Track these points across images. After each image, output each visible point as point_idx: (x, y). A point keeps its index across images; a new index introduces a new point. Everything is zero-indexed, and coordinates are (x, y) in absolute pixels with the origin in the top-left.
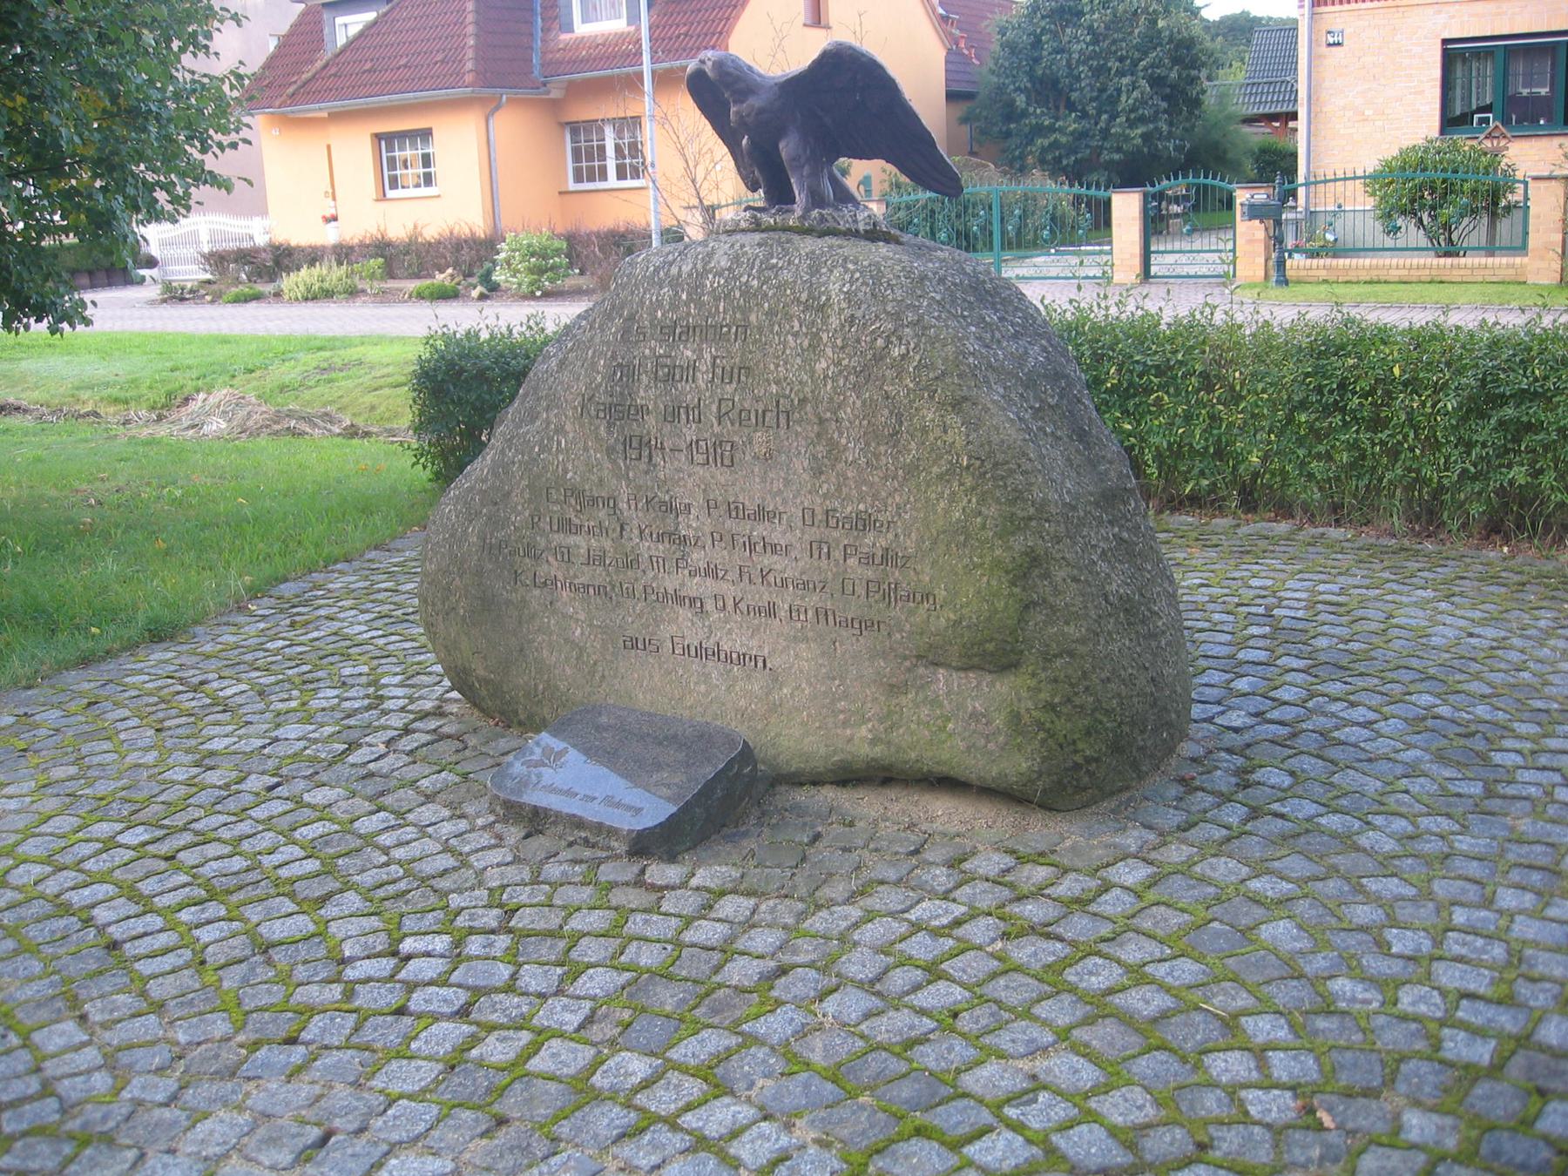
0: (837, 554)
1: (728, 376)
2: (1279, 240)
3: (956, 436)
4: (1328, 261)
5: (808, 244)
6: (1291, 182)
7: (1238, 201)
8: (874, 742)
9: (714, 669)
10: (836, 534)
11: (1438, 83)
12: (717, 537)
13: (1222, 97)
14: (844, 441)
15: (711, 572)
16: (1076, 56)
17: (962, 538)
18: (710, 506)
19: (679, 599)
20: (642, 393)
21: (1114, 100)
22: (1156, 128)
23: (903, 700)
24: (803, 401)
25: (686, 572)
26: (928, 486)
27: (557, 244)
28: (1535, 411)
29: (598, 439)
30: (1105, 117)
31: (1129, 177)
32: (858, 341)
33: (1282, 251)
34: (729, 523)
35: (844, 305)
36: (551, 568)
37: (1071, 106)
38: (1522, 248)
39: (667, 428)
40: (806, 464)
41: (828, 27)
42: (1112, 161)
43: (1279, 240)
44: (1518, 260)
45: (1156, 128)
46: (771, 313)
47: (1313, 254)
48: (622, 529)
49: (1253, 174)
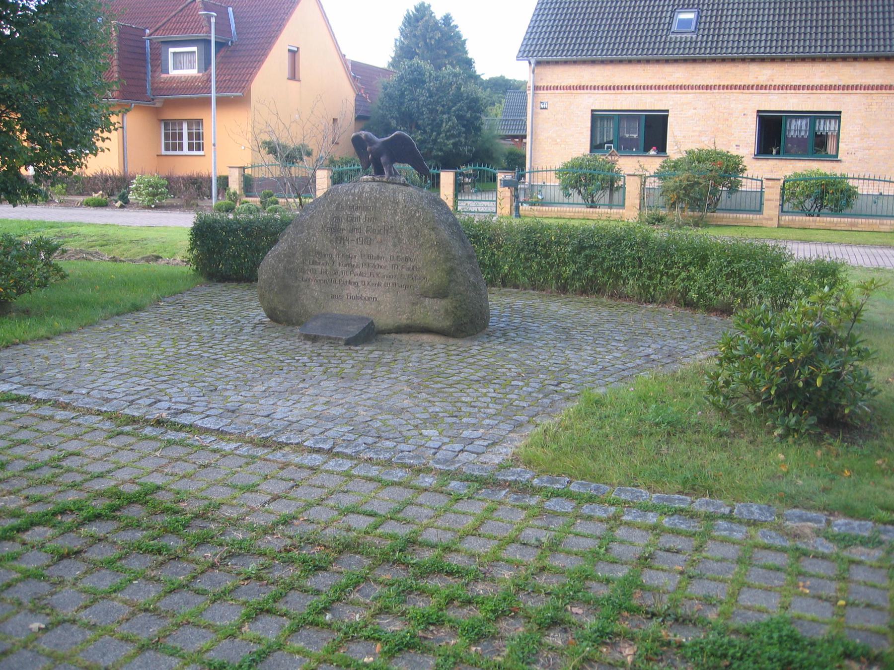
0: (400, 268)
1: (370, 220)
2: (517, 197)
3: (433, 236)
4: (539, 208)
5: (391, 186)
6: (523, 170)
7: (499, 178)
8: (408, 319)
11: (589, 129)
12: (364, 264)
13: (491, 128)
15: (361, 274)
16: (421, 103)
19: (350, 283)
21: (439, 126)
27: (163, 182)
28: (594, 252)
29: (327, 238)
30: (435, 133)
31: (447, 165)
33: (518, 202)
36: (309, 275)
37: (418, 127)
38: (623, 206)
41: (299, 81)
42: (438, 156)
43: (517, 197)
44: (621, 211)
46: (383, 204)
47: (533, 204)
49: (505, 165)
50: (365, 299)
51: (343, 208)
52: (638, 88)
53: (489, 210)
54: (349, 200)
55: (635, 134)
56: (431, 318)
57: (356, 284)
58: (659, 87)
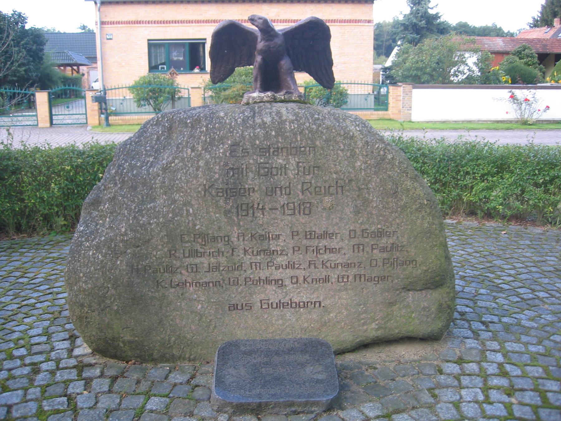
0: (368, 249)
9: (288, 313)
10: (367, 240)
11: (147, 54)
14: (371, 198)
15: (291, 265)
18: (294, 234)
19: (268, 281)
20: (250, 182)
22: (29, 68)
23: (394, 308)
24: (351, 181)
25: (273, 268)
26: (412, 214)
32: (372, 152)
34: (305, 242)
35: (362, 137)
39: (267, 199)
40: (352, 209)
46: (327, 141)
50: (298, 305)
51: (246, 152)
52: (182, 22)
53: (80, 121)
54: (256, 137)
55: (178, 56)
57: (279, 283)
58: (198, 22)
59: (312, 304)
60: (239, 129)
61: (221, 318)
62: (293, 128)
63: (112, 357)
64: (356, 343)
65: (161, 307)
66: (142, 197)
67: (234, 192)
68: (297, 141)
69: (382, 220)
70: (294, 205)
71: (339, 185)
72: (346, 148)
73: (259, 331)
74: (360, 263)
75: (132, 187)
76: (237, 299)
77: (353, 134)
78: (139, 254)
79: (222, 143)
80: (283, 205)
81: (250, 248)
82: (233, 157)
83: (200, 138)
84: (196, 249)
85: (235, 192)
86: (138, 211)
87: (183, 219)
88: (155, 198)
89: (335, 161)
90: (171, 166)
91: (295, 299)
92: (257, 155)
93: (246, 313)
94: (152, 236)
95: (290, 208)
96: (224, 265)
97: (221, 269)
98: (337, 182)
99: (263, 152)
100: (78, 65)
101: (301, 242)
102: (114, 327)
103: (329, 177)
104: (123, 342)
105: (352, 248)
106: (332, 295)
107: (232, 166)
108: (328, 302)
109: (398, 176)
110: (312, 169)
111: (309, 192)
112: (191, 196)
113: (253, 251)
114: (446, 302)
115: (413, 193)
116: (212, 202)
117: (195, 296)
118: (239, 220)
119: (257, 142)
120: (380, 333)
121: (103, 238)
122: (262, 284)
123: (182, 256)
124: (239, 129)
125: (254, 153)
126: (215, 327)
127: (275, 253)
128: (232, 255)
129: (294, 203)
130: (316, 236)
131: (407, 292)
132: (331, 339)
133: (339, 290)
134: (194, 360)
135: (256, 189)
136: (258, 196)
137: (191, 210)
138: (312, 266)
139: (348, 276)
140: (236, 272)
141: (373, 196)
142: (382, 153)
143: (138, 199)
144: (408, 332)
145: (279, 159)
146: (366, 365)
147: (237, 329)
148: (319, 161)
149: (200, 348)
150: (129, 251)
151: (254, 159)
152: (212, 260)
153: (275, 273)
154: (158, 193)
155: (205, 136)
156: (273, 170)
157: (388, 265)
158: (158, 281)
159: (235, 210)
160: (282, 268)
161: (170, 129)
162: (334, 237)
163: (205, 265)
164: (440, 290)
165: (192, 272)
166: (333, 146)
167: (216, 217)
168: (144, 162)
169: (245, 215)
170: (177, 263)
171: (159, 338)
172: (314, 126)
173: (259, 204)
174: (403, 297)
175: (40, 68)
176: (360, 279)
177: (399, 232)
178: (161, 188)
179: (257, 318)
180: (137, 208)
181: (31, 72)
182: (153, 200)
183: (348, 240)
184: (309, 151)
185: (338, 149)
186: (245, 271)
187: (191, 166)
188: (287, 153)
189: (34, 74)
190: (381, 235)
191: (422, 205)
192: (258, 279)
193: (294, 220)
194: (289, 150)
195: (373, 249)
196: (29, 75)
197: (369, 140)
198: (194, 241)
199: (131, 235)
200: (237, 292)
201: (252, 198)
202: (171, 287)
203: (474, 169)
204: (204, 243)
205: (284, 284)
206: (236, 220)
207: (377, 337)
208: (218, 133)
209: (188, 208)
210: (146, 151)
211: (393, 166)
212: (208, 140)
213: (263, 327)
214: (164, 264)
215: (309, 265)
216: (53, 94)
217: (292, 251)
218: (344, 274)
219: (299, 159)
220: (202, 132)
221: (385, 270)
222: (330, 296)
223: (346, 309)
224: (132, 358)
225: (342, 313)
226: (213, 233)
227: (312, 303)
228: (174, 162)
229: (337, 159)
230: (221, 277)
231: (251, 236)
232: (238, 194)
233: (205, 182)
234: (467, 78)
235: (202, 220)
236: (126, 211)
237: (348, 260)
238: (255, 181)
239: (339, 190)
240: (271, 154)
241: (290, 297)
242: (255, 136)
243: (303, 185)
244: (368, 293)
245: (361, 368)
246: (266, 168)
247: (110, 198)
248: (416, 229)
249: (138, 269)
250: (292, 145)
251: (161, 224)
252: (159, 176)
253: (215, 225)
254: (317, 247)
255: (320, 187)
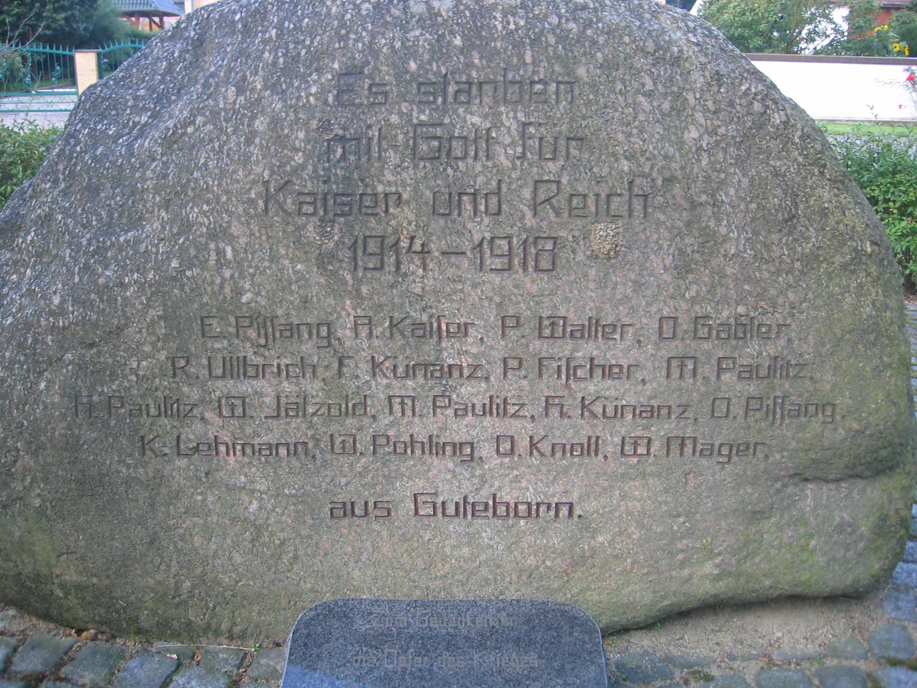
0: (707, 370)
10: (706, 346)
14: (723, 230)
17: (872, 337)
19: (435, 447)
20: (389, 177)
22: (73, 15)
23: (766, 525)
24: (669, 181)
25: (450, 412)
32: (731, 104)
34: (536, 345)
35: (703, 59)
40: (668, 261)
45: (73, 15)
46: (608, 66)
48: (341, 364)
51: (379, 91)
54: (410, 51)
56: (820, 559)
59: (549, 508)
60: (364, 29)
61: (310, 537)
62: (512, 27)
63: (46, 617)
64: (659, 611)
65: (152, 505)
66: (110, 216)
67: (344, 204)
68: (525, 64)
69: (749, 293)
70: (509, 243)
71: (636, 190)
72: (661, 88)
73: (408, 572)
74: (685, 407)
75: (88, 188)
76: (351, 488)
77: (681, 51)
78: (95, 365)
79: (317, 70)
80: (481, 244)
81: (387, 358)
82: (344, 106)
83: (260, 58)
84: (241, 355)
85: (350, 204)
86: (95, 252)
87: (207, 275)
88: (141, 218)
89: (628, 124)
90: (185, 133)
91: (507, 496)
92: (411, 102)
93: (376, 527)
94: (127, 318)
95: (499, 252)
96: (318, 400)
97: (311, 410)
98: (631, 183)
99: (427, 93)
100: (161, 15)
101: (527, 346)
102: (37, 549)
103: (611, 168)
104: (63, 586)
105: (665, 365)
106: (604, 489)
107: (341, 132)
108: (591, 506)
109: (798, 173)
110: (562, 142)
111: (553, 207)
112: (230, 214)
113: (395, 366)
114: (897, 511)
115: (838, 223)
116: (284, 231)
117: (243, 479)
118: (358, 282)
119: (413, 66)
120: (722, 587)
121: (10, 320)
122: (418, 452)
123: (206, 372)
124: (364, 29)
125: (403, 97)
126: (296, 557)
127: (456, 374)
128: (340, 374)
129: (509, 238)
130: (569, 330)
131: (801, 485)
132: (596, 597)
133: (623, 475)
134: (243, 636)
135: (405, 196)
136: (412, 217)
137: (229, 250)
138: (555, 412)
139: (650, 441)
140: (349, 421)
141: (729, 225)
142: (757, 106)
143: (100, 220)
144: (795, 585)
145: (472, 114)
146: (682, 666)
147: (351, 564)
148: (584, 123)
149: (256, 608)
150: (68, 356)
151: (401, 114)
152: (287, 386)
153: (455, 427)
154: (149, 204)
155: (275, 50)
156: (454, 143)
157: (758, 415)
158: (143, 438)
159: (349, 254)
160: (474, 414)
161: (199, 43)
162: (617, 336)
163: (267, 400)
164: (885, 480)
165: (233, 416)
166: (623, 82)
167: (296, 272)
168: (125, 126)
169: (375, 269)
170: (193, 393)
171: (151, 581)
172: (572, 25)
173: (412, 239)
174: (790, 496)
175: (92, 16)
176: (682, 450)
177: (793, 326)
178: (157, 190)
179: (404, 538)
180: (94, 242)
181: (77, 22)
182: (136, 222)
183: (656, 344)
184: (557, 93)
185: (638, 92)
186: (374, 417)
187: (234, 132)
188: (494, 97)
189: (82, 27)
190: (745, 332)
191: (858, 253)
192: (408, 439)
193: (509, 284)
194: (501, 91)
195: (720, 370)
196: (72, 28)
197: (723, 70)
198: (238, 336)
199: (74, 313)
200: (351, 470)
201: (393, 222)
202: (179, 454)
203: (886, 192)
204: (262, 341)
205: (476, 454)
206: (351, 282)
207: (716, 596)
208: (308, 42)
209: (222, 245)
210: (136, 98)
211: (787, 142)
212: (281, 60)
213: (419, 561)
214: (159, 393)
215: (546, 408)
216: (105, 55)
217: (500, 370)
218: (638, 434)
219: (527, 115)
220: (265, 42)
221: (749, 428)
222: (597, 489)
223: (640, 525)
224: (90, 626)
225: (629, 536)
226: (288, 315)
227: (549, 506)
228: (193, 123)
229: (635, 118)
230: (309, 433)
231: (391, 326)
232: (356, 208)
233: (266, 174)
234: (830, 44)
235: (257, 279)
236: (68, 251)
237: (650, 398)
238: (404, 175)
239: (638, 205)
240: (450, 99)
241: (493, 490)
242: (406, 48)
243: (535, 188)
244: (700, 485)
245: (671, 676)
246: (435, 138)
247: (39, 216)
248: (840, 320)
249: (90, 403)
250: (510, 76)
251: (150, 286)
252: (154, 160)
253: (291, 292)
254: (568, 360)
255: (585, 196)
